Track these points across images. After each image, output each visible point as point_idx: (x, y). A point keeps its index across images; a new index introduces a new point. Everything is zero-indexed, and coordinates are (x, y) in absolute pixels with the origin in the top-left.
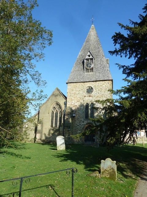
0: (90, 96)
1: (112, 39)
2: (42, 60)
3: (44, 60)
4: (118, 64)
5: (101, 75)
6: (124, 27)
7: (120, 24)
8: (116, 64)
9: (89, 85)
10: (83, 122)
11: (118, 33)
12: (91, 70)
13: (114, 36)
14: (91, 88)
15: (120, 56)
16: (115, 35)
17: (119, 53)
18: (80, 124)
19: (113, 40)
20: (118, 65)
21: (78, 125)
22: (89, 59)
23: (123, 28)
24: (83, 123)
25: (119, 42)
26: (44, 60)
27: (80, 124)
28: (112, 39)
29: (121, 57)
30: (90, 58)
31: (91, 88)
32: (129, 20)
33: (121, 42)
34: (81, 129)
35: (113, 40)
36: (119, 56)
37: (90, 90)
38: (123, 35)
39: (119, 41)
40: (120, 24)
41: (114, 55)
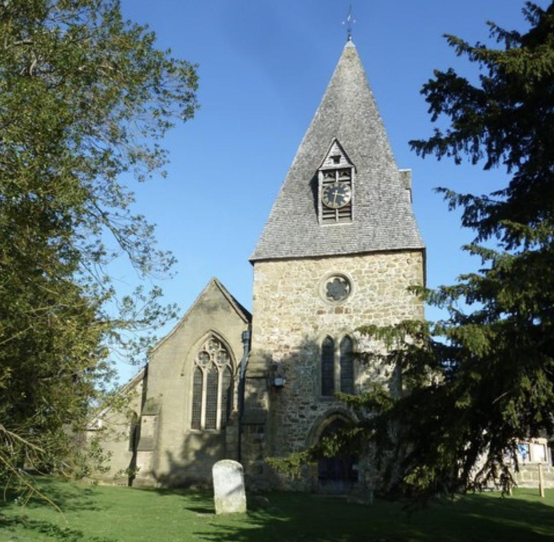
0: (339, 311)
5: (380, 231)
7: (452, 41)
10: (314, 408)
14: (342, 280)
15: (453, 158)
17: (450, 149)
22: (334, 170)
23: (465, 56)
24: (312, 413)
25: (450, 106)
30: (338, 166)
31: (342, 280)
32: (445, 36)
33: (457, 107)
37: (339, 288)
38: (463, 82)
39: (449, 101)
40: (452, 41)
41: (432, 157)
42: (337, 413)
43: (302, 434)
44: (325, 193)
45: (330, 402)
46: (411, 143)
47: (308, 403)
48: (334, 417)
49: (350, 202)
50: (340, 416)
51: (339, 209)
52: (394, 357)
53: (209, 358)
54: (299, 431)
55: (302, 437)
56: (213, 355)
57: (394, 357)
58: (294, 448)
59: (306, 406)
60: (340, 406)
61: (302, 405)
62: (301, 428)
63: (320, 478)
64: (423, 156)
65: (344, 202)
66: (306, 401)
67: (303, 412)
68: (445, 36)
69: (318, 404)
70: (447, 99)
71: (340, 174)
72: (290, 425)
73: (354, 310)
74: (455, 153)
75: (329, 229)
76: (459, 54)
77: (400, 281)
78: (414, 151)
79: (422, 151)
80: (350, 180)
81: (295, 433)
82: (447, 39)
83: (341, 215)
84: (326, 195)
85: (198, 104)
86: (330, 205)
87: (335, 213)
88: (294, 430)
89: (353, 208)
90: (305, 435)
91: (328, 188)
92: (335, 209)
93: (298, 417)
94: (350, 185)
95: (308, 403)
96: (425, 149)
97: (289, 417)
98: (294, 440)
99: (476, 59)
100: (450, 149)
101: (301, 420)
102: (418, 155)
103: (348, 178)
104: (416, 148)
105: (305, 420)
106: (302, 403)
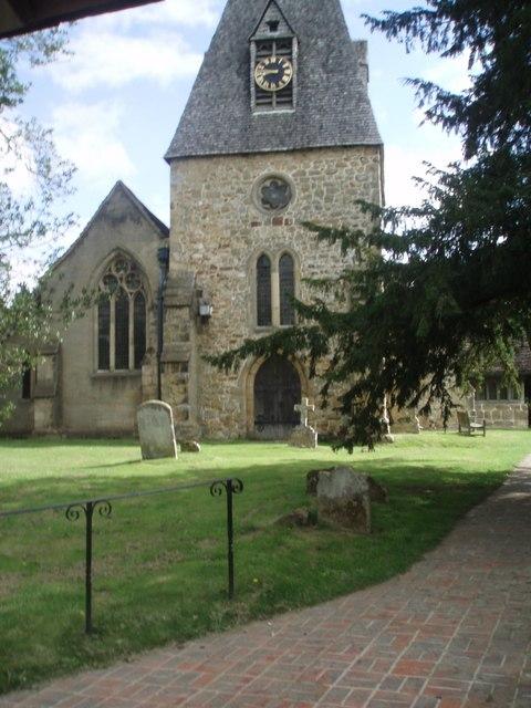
0: (277, 222)
22: (271, 40)
30: (276, 34)
80: (291, 54)
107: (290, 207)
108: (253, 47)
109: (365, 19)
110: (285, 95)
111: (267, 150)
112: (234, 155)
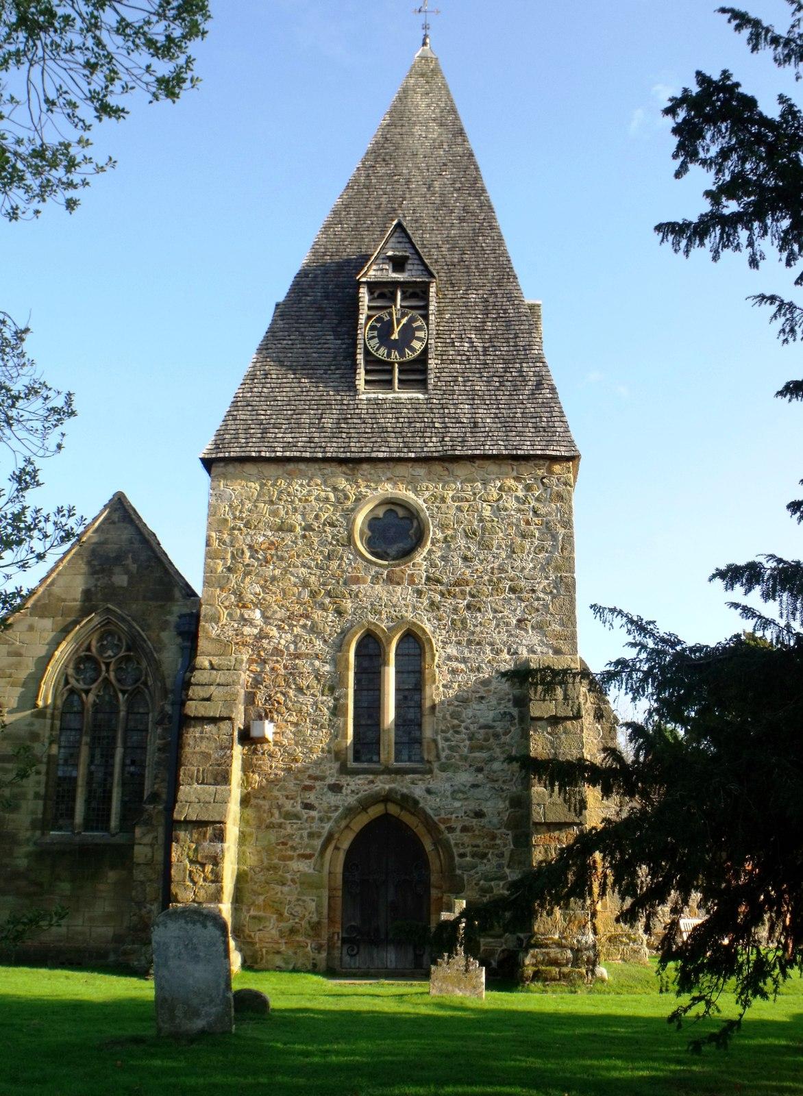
0: (390, 580)
1: (669, 122)
2: (54, 205)
3: (71, 204)
4: (772, 299)
5: (485, 417)
6: (775, 41)
7: (741, 19)
8: (762, 298)
9: (387, 489)
10: (336, 788)
11: (716, 77)
12: (405, 368)
13: (685, 99)
14: (401, 513)
15: (746, 253)
16: (695, 89)
17: (743, 234)
18: (308, 806)
19: (676, 131)
20: (774, 308)
21: (288, 816)
22: (396, 284)
23: (767, 52)
24: (333, 799)
25: (714, 150)
26: (71, 204)
27: (308, 806)
28: (669, 122)
29: (754, 263)
30: (400, 277)
31: (401, 513)
32: (723, 10)
33: (724, 154)
34: (318, 843)
35: (676, 131)
36: (735, 259)
37: (397, 534)
38: (751, 103)
39: (713, 140)
40: (741, 19)
41: (701, 253)
42: (387, 798)
43: (307, 846)
44: (372, 328)
45: (371, 777)
46: (659, 228)
47: (323, 779)
48: (375, 811)
49: (425, 351)
50: (393, 809)
51: (400, 364)
52: (617, 674)
53: (97, 670)
54: (302, 837)
55: (308, 851)
56: (108, 665)
57: (617, 674)
58: (289, 876)
59: (318, 784)
60: (393, 785)
61: (307, 783)
62: (305, 833)
63: (344, 941)
64: (687, 252)
65: (413, 350)
66: (318, 773)
67: (311, 797)
68: (723, 10)
69: (344, 780)
70: (708, 135)
71: (403, 293)
72: (280, 826)
73: (428, 578)
74: (751, 244)
75: (376, 403)
76: (755, 48)
77: (528, 523)
78: (668, 245)
79: (684, 243)
80: (426, 307)
81: (290, 843)
82: (728, 16)
83: (404, 377)
84: (376, 333)
85: (669, 118)
86: (382, 353)
87: (391, 372)
88: (290, 836)
89: (432, 363)
90: (313, 848)
91: (379, 320)
92: (392, 364)
93: (299, 808)
94: (426, 317)
95: (323, 779)
96: (690, 240)
97: (279, 807)
98: (291, 858)
99: (787, 58)
100: (743, 234)
101: (305, 814)
102: (676, 251)
103: (422, 304)
104: (671, 237)
105: (314, 813)
106: (310, 777)
107: (420, 557)
108: (364, 293)
109: (728, 16)
110: (416, 372)
111: (381, 455)
112: (325, 460)
